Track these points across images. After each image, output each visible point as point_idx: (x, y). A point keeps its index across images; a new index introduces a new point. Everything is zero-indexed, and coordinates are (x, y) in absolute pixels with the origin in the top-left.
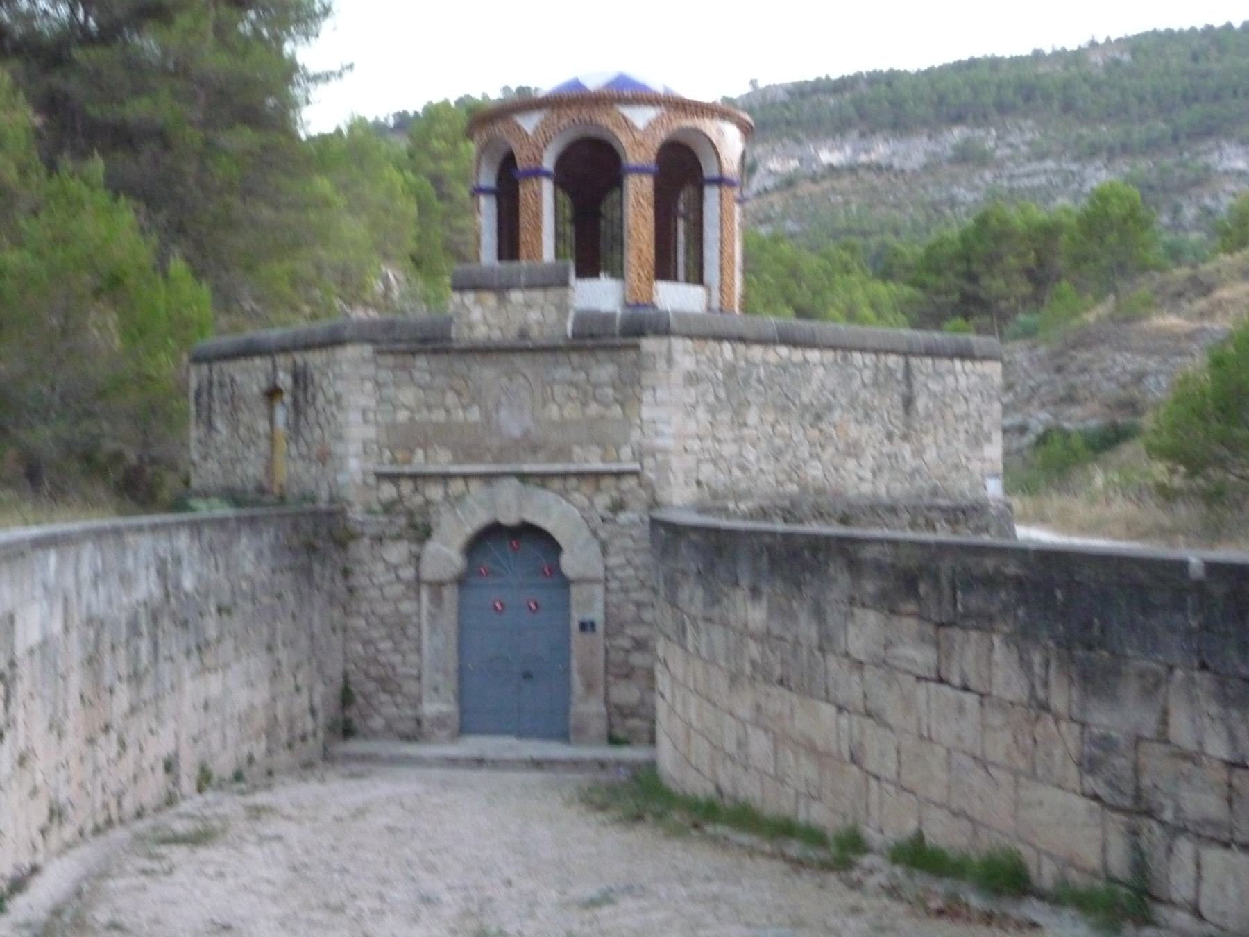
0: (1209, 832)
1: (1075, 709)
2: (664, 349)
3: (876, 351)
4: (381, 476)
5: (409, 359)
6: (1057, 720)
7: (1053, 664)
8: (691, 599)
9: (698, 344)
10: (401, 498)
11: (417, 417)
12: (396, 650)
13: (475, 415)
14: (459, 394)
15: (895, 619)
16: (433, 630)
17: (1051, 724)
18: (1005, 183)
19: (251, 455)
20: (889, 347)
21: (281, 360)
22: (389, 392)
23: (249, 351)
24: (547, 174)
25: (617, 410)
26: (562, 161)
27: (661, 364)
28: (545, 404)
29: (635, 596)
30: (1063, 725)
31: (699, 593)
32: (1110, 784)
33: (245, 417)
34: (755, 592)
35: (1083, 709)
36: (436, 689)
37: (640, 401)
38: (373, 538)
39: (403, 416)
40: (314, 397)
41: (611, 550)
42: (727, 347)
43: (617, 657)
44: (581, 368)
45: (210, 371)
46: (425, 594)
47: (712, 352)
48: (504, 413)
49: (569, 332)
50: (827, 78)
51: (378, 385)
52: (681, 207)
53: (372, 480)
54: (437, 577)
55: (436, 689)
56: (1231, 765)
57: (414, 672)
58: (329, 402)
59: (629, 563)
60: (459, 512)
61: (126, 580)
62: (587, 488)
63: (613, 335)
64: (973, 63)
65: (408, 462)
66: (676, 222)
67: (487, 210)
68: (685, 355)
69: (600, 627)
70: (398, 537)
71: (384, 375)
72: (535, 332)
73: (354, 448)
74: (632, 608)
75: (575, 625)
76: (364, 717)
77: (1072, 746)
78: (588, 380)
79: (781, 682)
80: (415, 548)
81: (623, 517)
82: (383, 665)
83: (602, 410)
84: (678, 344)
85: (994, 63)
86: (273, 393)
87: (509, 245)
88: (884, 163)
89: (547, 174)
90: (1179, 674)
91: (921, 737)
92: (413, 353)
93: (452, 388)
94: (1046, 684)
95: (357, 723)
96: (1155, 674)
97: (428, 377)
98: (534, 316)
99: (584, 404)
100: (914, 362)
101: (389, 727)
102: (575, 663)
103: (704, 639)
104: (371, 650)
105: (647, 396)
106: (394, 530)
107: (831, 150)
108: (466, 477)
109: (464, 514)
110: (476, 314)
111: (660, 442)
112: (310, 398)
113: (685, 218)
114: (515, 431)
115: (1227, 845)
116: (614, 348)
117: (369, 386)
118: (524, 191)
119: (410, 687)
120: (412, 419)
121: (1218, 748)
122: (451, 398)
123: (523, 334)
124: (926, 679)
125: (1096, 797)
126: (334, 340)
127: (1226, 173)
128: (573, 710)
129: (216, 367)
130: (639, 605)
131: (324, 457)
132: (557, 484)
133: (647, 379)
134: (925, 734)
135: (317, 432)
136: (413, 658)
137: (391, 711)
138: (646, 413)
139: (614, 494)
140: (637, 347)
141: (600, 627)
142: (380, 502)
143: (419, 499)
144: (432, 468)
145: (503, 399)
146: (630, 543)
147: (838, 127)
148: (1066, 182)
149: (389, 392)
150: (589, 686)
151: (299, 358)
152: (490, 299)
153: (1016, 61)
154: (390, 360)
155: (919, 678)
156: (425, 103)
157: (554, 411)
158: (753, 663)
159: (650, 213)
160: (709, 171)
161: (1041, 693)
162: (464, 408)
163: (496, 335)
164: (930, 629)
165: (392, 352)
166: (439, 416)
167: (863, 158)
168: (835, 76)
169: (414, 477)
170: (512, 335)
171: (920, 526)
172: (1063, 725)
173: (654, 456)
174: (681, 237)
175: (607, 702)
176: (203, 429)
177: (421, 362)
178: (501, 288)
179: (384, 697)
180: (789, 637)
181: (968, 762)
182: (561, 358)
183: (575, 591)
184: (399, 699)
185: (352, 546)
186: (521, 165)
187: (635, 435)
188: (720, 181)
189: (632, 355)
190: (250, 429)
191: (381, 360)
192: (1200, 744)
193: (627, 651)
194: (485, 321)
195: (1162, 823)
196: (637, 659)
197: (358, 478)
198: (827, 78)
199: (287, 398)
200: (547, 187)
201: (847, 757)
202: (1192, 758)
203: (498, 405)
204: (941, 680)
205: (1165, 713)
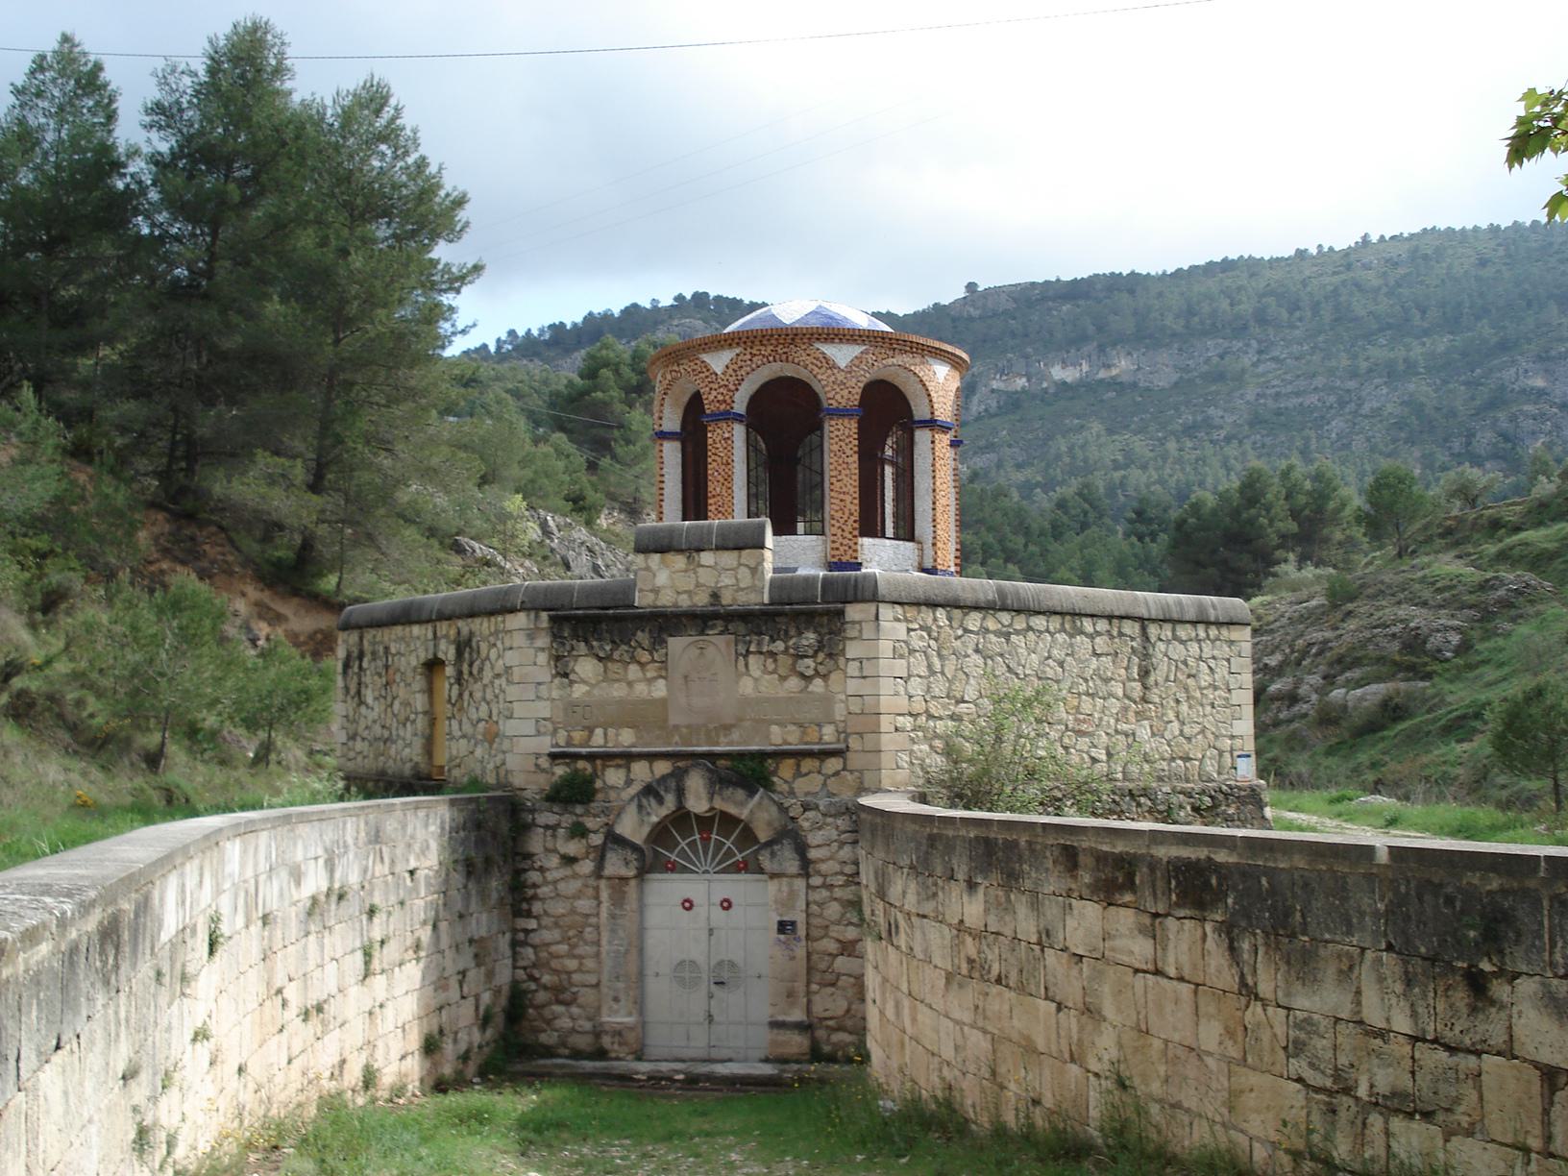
0: (1395, 1103)
1: (1280, 994)
3: (1110, 617)
4: (554, 757)
6: (1264, 1006)
7: (1261, 952)
8: (904, 893)
9: (911, 612)
15: (1112, 909)
17: (1259, 1009)
18: (1270, 403)
19: (408, 732)
20: (1123, 614)
21: (443, 628)
23: (405, 616)
24: (738, 418)
26: (754, 400)
29: (838, 893)
30: (1270, 1010)
31: (913, 886)
32: (1311, 1065)
33: (402, 691)
34: (972, 886)
35: (1288, 995)
40: (481, 670)
42: (941, 613)
45: (361, 638)
50: (1058, 280)
52: (889, 452)
53: (544, 762)
55: (616, 999)
56: (1415, 1039)
58: (498, 676)
61: (297, 876)
64: (1227, 265)
65: (586, 743)
66: (883, 470)
67: (672, 452)
68: (893, 625)
72: (726, 599)
77: (1280, 1030)
79: (999, 981)
84: (886, 612)
85: (1250, 266)
86: (433, 665)
87: (695, 502)
88: (1125, 379)
89: (738, 418)
90: (1369, 955)
91: (1140, 1031)
94: (1255, 971)
96: (1350, 957)
98: (727, 580)
100: (1153, 630)
103: (918, 934)
107: (1065, 364)
112: (475, 671)
113: (893, 464)
115: (1410, 1115)
118: (715, 435)
119: (587, 996)
121: (1402, 1024)
124: (1145, 972)
125: (1300, 1080)
126: (501, 607)
127: (1523, 391)
129: (370, 635)
131: (492, 737)
134: (1144, 1028)
135: (484, 707)
137: (565, 1023)
140: (841, 613)
141: (802, 931)
147: (1071, 344)
148: (1342, 404)
151: (464, 626)
152: (679, 561)
153: (1275, 262)
155: (1137, 971)
156: (585, 313)
158: (970, 961)
159: (854, 460)
160: (920, 412)
161: (1250, 981)
163: (684, 602)
164: (1147, 920)
167: (1102, 374)
168: (1067, 277)
170: (702, 600)
171: (45, 854)
172: (1270, 1010)
174: (889, 494)
176: (351, 704)
178: (693, 548)
179: (559, 1009)
180: (1008, 931)
181: (1181, 1052)
184: (575, 1010)
186: (709, 408)
188: (932, 424)
190: (406, 704)
192: (1388, 1020)
195: (1357, 1099)
196: (842, 963)
198: (1058, 280)
199: (449, 671)
200: (739, 432)
201: (1067, 1056)
202: (1382, 1034)
204: (1157, 972)
205: (1358, 993)
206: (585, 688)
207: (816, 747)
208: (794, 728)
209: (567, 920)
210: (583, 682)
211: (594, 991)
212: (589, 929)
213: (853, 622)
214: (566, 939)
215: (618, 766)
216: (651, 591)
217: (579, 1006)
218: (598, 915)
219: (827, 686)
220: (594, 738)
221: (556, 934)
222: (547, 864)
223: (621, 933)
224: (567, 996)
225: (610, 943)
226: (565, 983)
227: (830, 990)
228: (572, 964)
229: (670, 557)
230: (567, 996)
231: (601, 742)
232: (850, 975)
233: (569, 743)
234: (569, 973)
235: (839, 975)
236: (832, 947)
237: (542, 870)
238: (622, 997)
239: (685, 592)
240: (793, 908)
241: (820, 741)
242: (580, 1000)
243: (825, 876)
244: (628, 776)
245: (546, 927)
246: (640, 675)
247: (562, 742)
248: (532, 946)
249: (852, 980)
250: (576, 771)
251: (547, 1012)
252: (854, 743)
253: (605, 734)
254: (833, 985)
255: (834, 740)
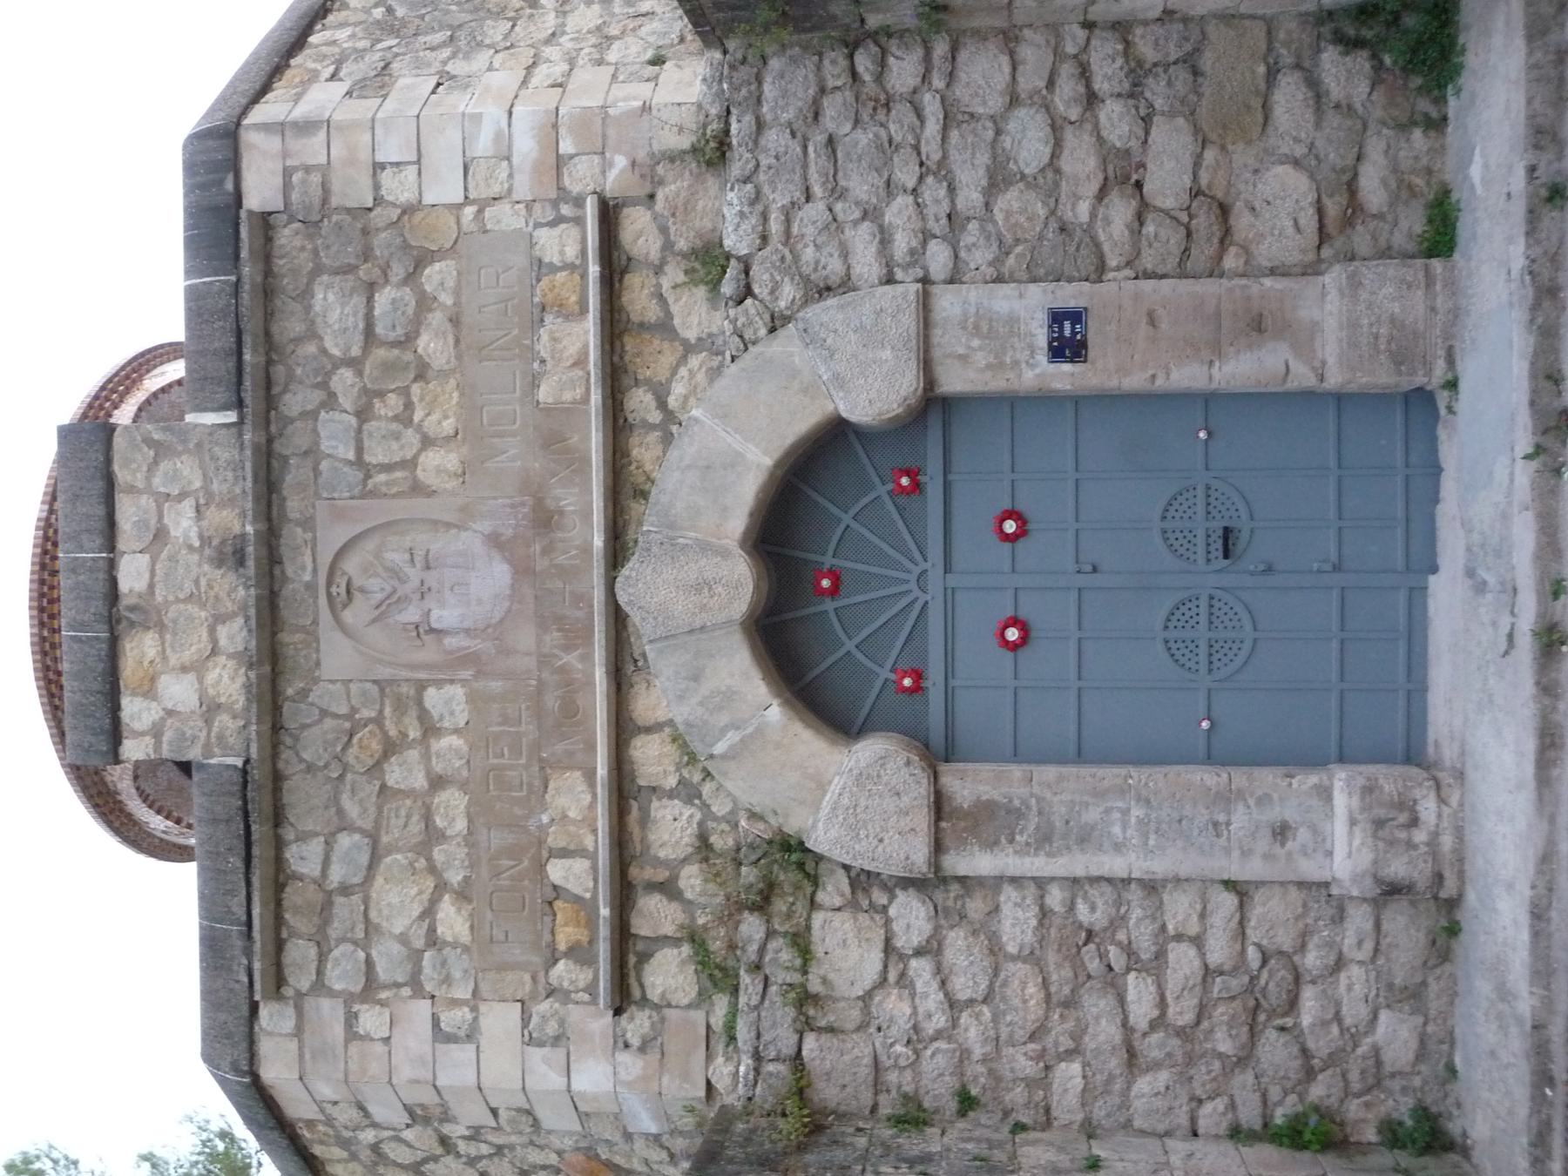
2: (273, 143)
4: (623, 997)
5: (293, 896)
10: (694, 937)
11: (455, 877)
12: (1157, 965)
13: (449, 702)
14: (391, 748)
16: (1085, 839)
22: (388, 960)
25: (437, 275)
27: (313, 150)
28: (417, 489)
29: (970, 197)
36: (1282, 832)
37: (409, 210)
38: (805, 1025)
39: (453, 921)
41: (834, 267)
43: (1162, 239)
44: (324, 385)
46: (962, 862)
47: (489, 186)
48: (445, 615)
49: (231, 417)
51: (370, 987)
53: (637, 1024)
54: (922, 820)
55: (1282, 832)
57: (1226, 902)
59: (869, 214)
60: (719, 748)
62: (652, 359)
63: (237, 285)
65: (585, 907)
69: (1069, 295)
70: (801, 943)
71: (343, 973)
73: (545, 1073)
74: (1010, 200)
75: (1064, 376)
76: (1377, 1076)
78: (355, 364)
80: (833, 890)
81: (736, 240)
82: (1202, 1012)
83: (436, 318)
92: (280, 879)
93: (376, 768)
95: (1401, 1107)
97: (344, 841)
98: (183, 524)
99: (422, 373)
101: (1411, 996)
102: (1187, 376)
104: (1154, 1046)
105: (399, 188)
106: (782, 954)
108: (623, 729)
109: (724, 731)
110: (179, 692)
111: (525, 146)
114: (494, 577)
116: (267, 292)
117: (371, 1020)
120: (463, 895)
122: (405, 773)
123: (231, 555)
128: (1334, 379)
130: (998, 179)
132: (643, 450)
133: (353, 190)
136: (1180, 909)
137: (1355, 984)
138: (444, 188)
139: (674, 274)
140: (265, 221)
142: (703, 998)
143: (691, 880)
144: (599, 841)
145: (412, 614)
146: (815, 211)
149: (388, 960)
150: (1258, 326)
152: (140, 650)
154: (300, 952)
157: (437, 464)
162: (430, 729)
163: (234, 635)
165: (279, 946)
166: (452, 809)
169: (624, 894)
170: (235, 590)
173: (560, 162)
175: (1312, 269)
177: (304, 858)
179: (1310, 1007)
182: (293, 442)
183: (953, 381)
184: (1312, 960)
185: (827, 1093)
187: (506, 218)
189: (287, 237)
191: (300, 980)
193: (1143, 210)
194: (195, 668)
197: (631, 1065)
203: (425, 631)
206: (447, 909)
207: (594, 269)
208: (544, 334)
209: (1060, 976)
210: (429, 912)
211: (1258, 897)
212: (1082, 909)
213: (287, 187)
214: (1113, 982)
215: (645, 820)
216: (208, 722)
217: (1302, 948)
218: (1041, 883)
219: (665, 940)
220: (574, 887)
221: (1096, 1004)
222: (903, 1024)
223: (1092, 815)
224: (1275, 982)
225: (1118, 848)
226: (1237, 983)
227: (1242, 222)
228: (1183, 961)
229: (129, 668)
230: (1275, 982)
231: (580, 865)
232: (1197, 164)
233: (581, 954)
234: (1208, 973)
235: (1196, 193)
236: (1120, 211)
237: (916, 1038)
238: (1274, 814)
239: (212, 631)
240: (1012, 320)
241: (579, 269)
242: (1285, 940)
243: (926, 236)
244: (671, 794)
245: (1077, 1036)
246: (413, 755)
247: (583, 976)
248: (955, 1023)
249: (1210, 155)
250: (263, 998)
251: (1320, 1046)
252: (582, 177)
253: (564, 853)
254: (1224, 210)
255: (573, 232)
